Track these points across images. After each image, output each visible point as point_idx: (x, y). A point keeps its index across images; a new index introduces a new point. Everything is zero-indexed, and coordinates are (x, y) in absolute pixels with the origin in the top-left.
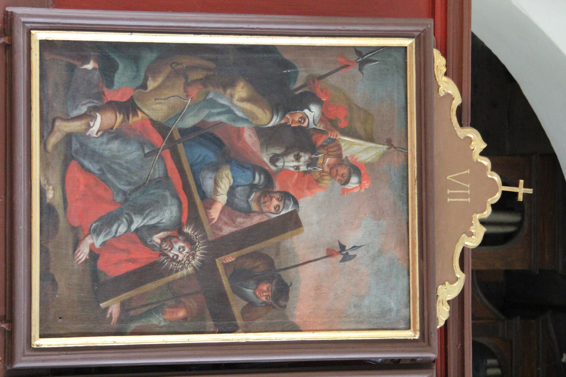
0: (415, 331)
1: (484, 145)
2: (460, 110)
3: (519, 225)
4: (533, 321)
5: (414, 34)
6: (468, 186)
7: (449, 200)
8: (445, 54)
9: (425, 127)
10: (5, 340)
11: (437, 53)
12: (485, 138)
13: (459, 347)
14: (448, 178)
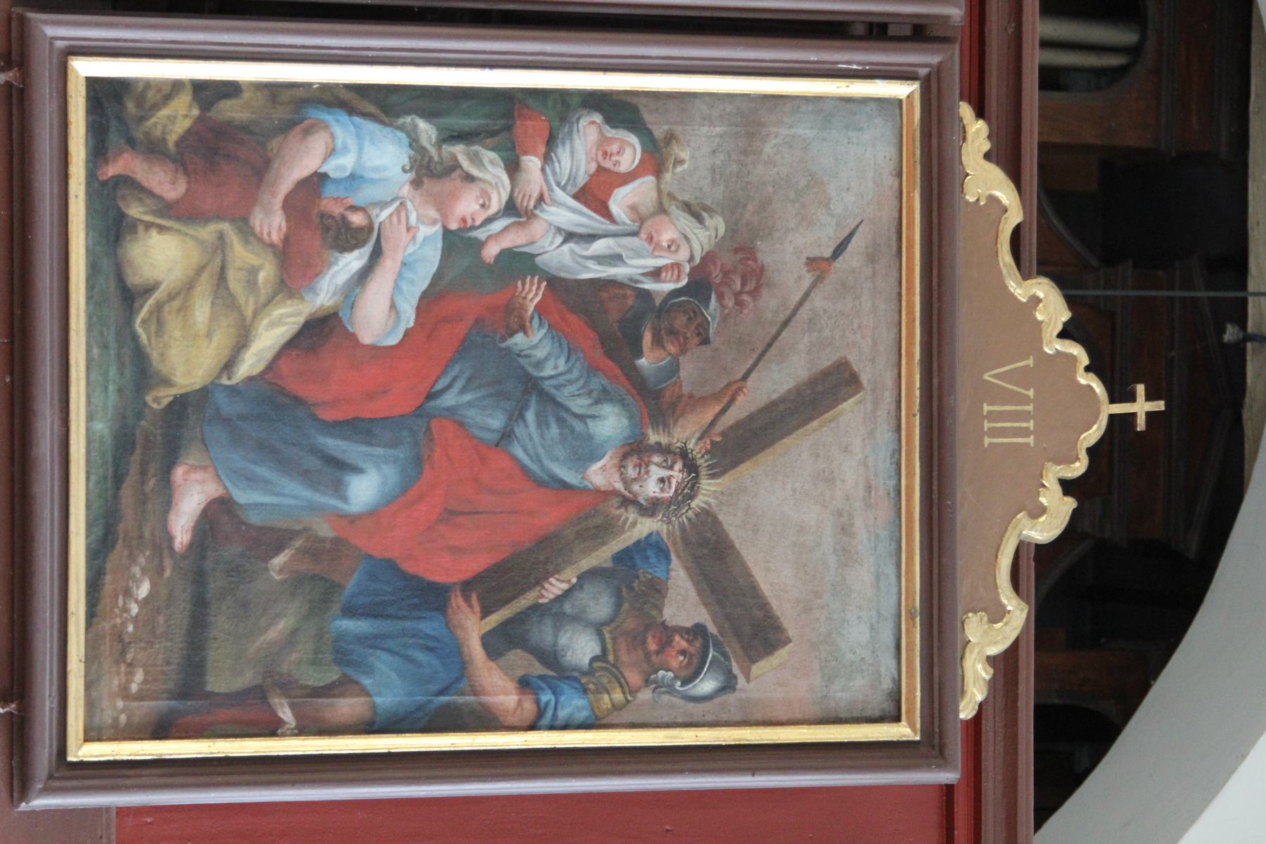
0: (912, 725)
1: (1065, 315)
2: (1017, 233)
3: (1134, 51)
4: (1160, 273)
5: (917, 73)
6: (1031, 393)
7: (987, 440)
8: (980, 113)
9: (940, 627)
10: (12, 591)
11: (966, 111)
12: (1071, 301)
13: (1011, 31)
14: (986, 377)
